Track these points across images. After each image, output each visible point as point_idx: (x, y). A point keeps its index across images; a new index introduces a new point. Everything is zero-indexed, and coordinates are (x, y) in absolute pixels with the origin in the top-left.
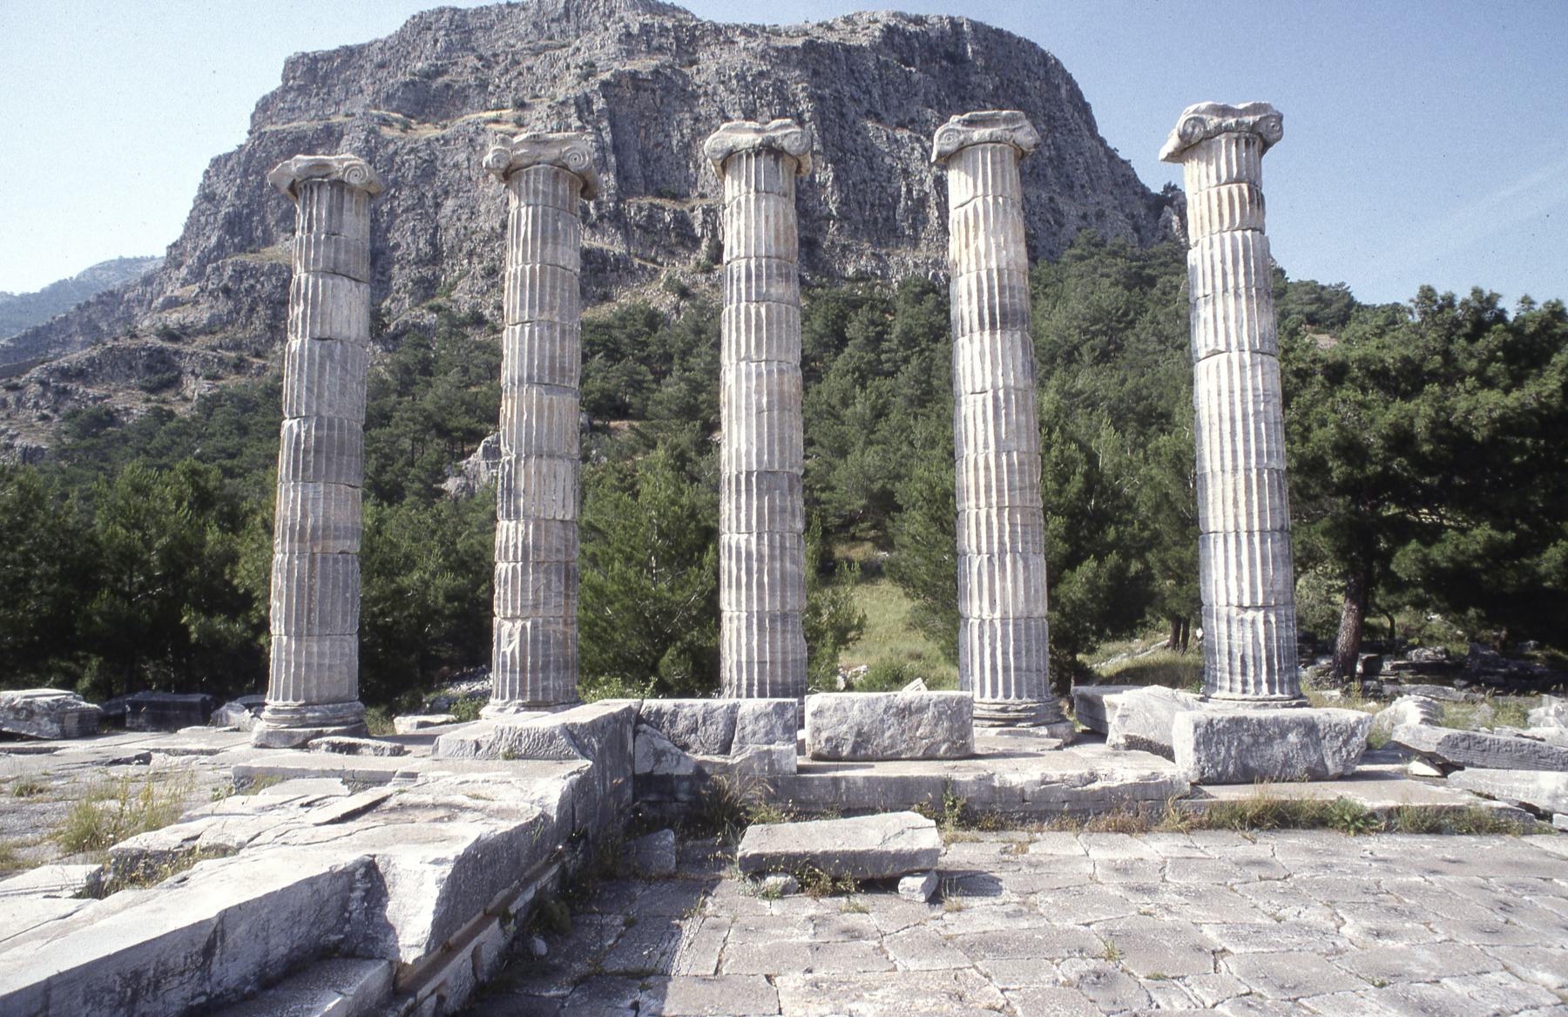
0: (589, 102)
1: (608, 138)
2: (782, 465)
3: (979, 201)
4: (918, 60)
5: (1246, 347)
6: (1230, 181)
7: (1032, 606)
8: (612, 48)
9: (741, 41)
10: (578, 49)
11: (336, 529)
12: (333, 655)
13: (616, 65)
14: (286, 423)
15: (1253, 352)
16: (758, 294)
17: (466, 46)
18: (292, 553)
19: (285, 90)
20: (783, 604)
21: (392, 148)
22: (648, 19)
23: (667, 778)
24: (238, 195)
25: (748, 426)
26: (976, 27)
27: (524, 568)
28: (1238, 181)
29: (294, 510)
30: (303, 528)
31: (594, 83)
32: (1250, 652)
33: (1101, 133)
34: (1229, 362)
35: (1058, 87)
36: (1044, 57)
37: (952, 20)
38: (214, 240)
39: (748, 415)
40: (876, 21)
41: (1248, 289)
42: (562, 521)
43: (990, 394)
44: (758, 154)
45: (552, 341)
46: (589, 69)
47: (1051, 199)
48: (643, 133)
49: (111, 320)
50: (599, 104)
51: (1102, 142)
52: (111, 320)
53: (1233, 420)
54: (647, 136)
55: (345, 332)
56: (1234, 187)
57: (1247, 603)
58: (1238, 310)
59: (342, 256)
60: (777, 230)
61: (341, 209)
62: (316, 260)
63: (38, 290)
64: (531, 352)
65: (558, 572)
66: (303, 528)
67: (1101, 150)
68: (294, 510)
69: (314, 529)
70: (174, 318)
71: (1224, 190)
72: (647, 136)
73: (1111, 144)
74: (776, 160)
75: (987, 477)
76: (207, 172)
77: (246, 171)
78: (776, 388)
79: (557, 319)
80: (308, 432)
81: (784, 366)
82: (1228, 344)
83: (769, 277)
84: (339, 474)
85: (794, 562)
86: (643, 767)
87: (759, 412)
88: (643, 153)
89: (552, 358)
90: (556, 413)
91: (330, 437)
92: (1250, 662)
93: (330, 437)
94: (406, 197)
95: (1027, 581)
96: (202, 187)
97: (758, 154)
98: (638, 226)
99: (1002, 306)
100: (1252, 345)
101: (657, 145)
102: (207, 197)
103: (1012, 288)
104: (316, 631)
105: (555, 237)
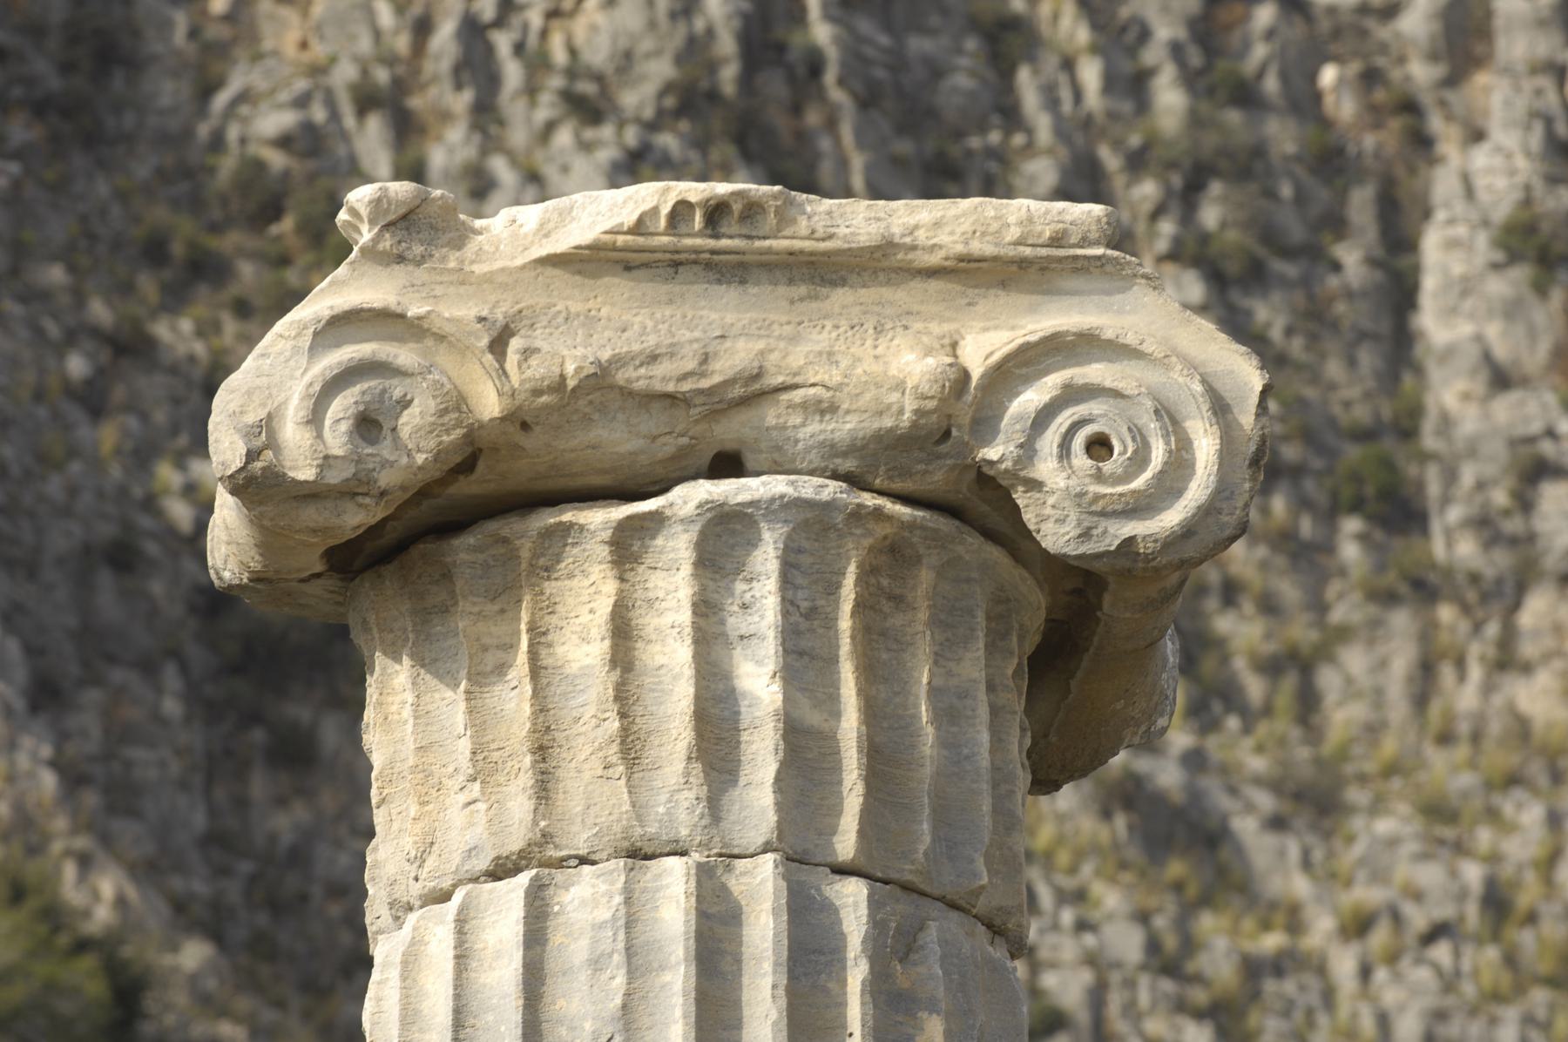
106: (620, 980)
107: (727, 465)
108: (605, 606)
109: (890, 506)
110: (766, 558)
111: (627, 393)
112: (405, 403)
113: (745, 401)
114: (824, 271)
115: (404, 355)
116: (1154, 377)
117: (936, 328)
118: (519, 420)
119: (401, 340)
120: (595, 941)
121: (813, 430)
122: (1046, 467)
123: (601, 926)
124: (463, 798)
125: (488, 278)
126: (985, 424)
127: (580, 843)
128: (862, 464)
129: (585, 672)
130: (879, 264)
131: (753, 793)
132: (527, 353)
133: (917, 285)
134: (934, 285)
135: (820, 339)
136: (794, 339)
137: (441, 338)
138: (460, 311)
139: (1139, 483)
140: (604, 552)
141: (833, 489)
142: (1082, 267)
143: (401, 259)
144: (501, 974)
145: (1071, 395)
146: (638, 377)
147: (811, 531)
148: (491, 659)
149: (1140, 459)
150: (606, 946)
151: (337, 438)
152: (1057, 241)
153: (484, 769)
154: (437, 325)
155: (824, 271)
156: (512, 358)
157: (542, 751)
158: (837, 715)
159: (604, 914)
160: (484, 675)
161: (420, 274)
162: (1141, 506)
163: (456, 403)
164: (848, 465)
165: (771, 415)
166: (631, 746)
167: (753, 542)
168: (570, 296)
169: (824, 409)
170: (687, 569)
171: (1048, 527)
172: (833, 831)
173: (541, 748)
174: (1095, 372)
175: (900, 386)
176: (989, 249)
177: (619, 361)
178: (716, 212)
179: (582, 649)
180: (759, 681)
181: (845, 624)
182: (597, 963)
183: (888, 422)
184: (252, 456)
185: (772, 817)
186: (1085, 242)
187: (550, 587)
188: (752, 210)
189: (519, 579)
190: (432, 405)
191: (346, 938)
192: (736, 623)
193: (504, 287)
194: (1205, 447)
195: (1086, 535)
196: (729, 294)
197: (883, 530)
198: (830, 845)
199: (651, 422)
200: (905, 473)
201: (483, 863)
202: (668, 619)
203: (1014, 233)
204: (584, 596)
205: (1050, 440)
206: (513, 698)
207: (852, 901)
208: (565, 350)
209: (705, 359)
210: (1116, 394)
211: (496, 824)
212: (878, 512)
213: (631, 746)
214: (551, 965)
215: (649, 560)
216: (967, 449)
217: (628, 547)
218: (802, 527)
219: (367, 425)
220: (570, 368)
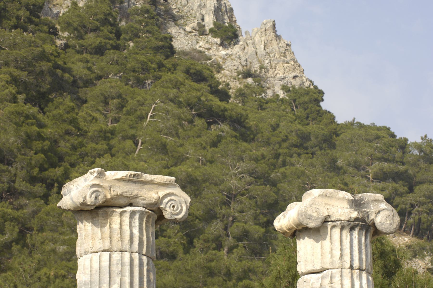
106: (120, 267)
107: (131, 205)
108: (119, 221)
109: (150, 212)
110: (137, 217)
111: (124, 196)
112: (100, 195)
113: (135, 198)
114: (144, 183)
115: (100, 190)
116: (179, 198)
117: (156, 191)
118: (112, 199)
119: (99, 187)
120: (117, 262)
121: (142, 202)
122: (168, 209)
123: (118, 260)
124: (99, 241)
125: (108, 181)
126: (161, 203)
127: (115, 249)
128: (146, 206)
129: (116, 228)
130: (151, 183)
131: (135, 245)
132: (114, 191)
133: (154, 185)
134: (156, 185)
135: (144, 191)
136: (141, 191)
137: (104, 188)
138: (106, 185)
139: (178, 211)
140: (119, 215)
141: (144, 209)
142: (172, 185)
143: (99, 178)
144: (105, 264)
145: (171, 200)
146: (125, 194)
147: (142, 214)
148: (103, 225)
149: (178, 209)
150: (119, 262)
151: (93, 200)
152: (170, 182)
153: (102, 238)
154: (104, 186)
155: (144, 183)
156: (112, 191)
157: (110, 238)
158: (143, 236)
159: (118, 258)
160: (103, 226)
161: (101, 180)
162: (177, 214)
163: (105, 196)
164: (145, 206)
165: (138, 200)
166: (121, 238)
167: (135, 215)
168: (117, 184)
169: (144, 200)
170: (128, 218)
171: (166, 215)
172: (143, 250)
173: (181, 273)
174: (173, 197)
175: (153, 198)
176: (162, 182)
177: (123, 192)
178: (134, 175)
179: (116, 225)
180: (136, 231)
181: (144, 225)
182: (117, 264)
183: (151, 202)
184: (84, 201)
185: (137, 249)
186: (173, 182)
187: (111, 218)
188: (138, 175)
189: (107, 216)
190: (103, 196)
191: (73, 250)
192: (133, 224)
193: (110, 182)
194: (184, 208)
195: (171, 217)
196: (134, 185)
197: (148, 214)
198: (142, 252)
199: (125, 200)
200: (151, 207)
201: (102, 250)
202: (126, 223)
203: (165, 180)
204: (115, 220)
205: (168, 205)
206: (107, 229)
207: (145, 258)
209: (132, 193)
210: (175, 200)
211: (104, 245)
212: (148, 212)
213: (121, 238)
214: (111, 264)
215: (123, 216)
216: (159, 205)
217: (122, 214)
218: (141, 213)
219: (96, 198)
220: (119, 193)
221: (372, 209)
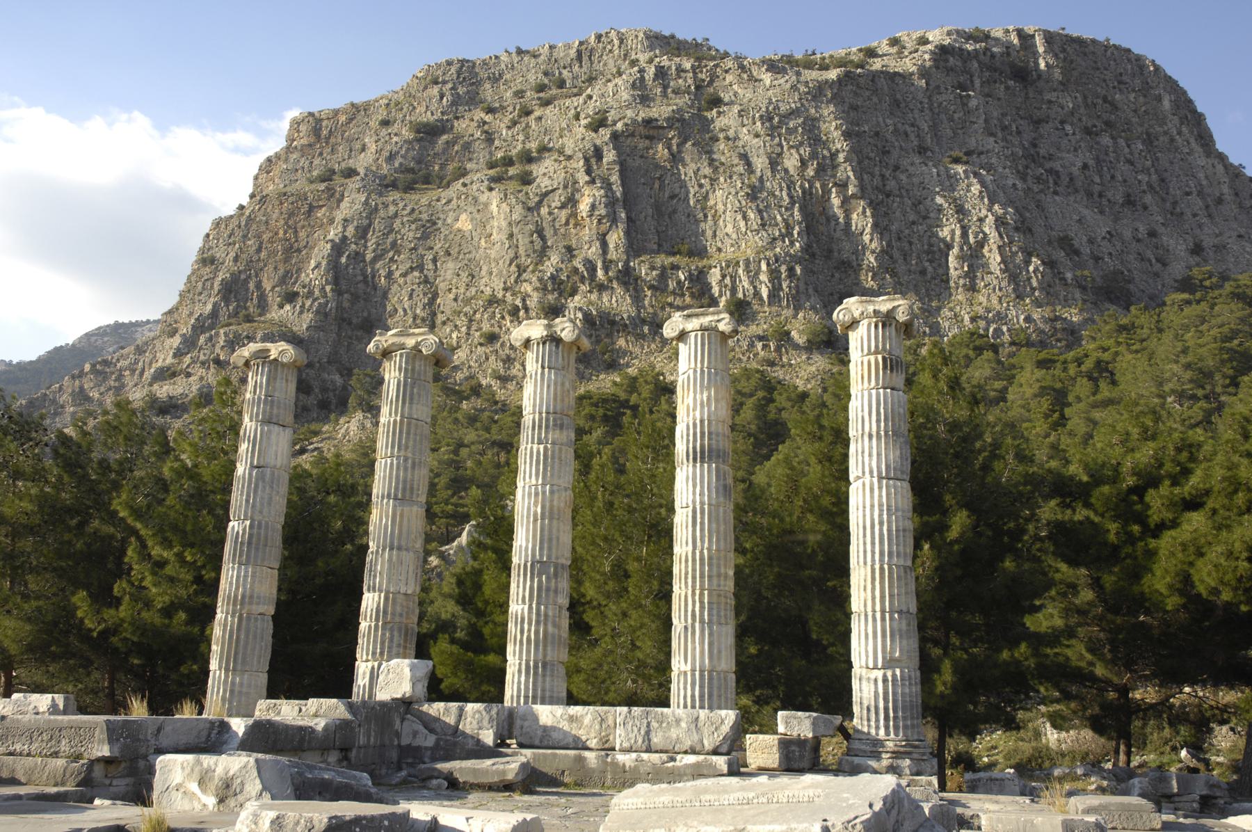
0: (598, 153)
1: (618, 190)
2: (549, 557)
3: (691, 372)
4: (977, 83)
5: (875, 474)
6: (869, 353)
7: (715, 662)
8: (625, 96)
9: (767, 78)
10: (590, 97)
11: (259, 597)
12: (249, 686)
13: (629, 113)
14: (231, 524)
15: (880, 478)
16: (539, 439)
17: (473, 100)
18: (227, 613)
19: (289, 149)
20: (545, 656)
21: (392, 209)
22: (665, 60)
23: (419, 748)
24: (236, 259)
25: (528, 530)
26: (1050, 38)
27: (376, 626)
28: (876, 352)
29: (231, 583)
30: (236, 596)
31: (605, 133)
32: (873, 703)
33: (1221, 146)
34: (864, 485)
35: (1159, 99)
36: (1139, 62)
37: (1020, 33)
38: (209, 307)
39: (528, 522)
40: (926, 42)
41: (886, 433)
42: (405, 594)
43: (690, 509)
44: (544, 343)
45: (406, 469)
46: (599, 123)
47: (1152, 234)
48: (657, 186)
49: (102, 389)
50: (610, 156)
51: (1222, 158)
52: (102, 389)
53: (864, 528)
54: (662, 188)
55: (272, 463)
56: (872, 358)
57: (871, 665)
58: (871, 448)
59: (275, 411)
60: (555, 394)
61: (275, 379)
62: (257, 414)
63: (34, 359)
64: (390, 478)
65: (400, 630)
66: (236, 596)
67: (1220, 168)
68: (231, 583)
69: (243, 597)
70: (164, 391)
71: (866, 359)
72: (662, 188)
73: (1234, 160)
74: (557, 346)
75: (687, 567)
76: (208, 235)
77: (245, 236)
78: (548, 504)
79: (410, 455)
80: (244, 530)
81: (555, 488)
82: (864, 473)
83: (547, 427)
84: (263, 560)
85: (554, 625)
86: (405, 741)
87: (535, 520)
88: (657, 207)
89: (405, 481)
90: (405, 519)
91: (259, 534)
92: (873, 709)
93: (259, 534)
94: (404, 262)
95: (710, 644)
96: (202, 251)
97: (544, 343)
98: (651, 287)
99: (709, 445)
100: (879, 472)
101: (672, 197)
102: (207, 260)
103: (717, 435)
104: (239, 667)
105: (411, 399)
130: (413, 334)
155: (409, 335)
208: (390, 342)
221: (558, 330)
